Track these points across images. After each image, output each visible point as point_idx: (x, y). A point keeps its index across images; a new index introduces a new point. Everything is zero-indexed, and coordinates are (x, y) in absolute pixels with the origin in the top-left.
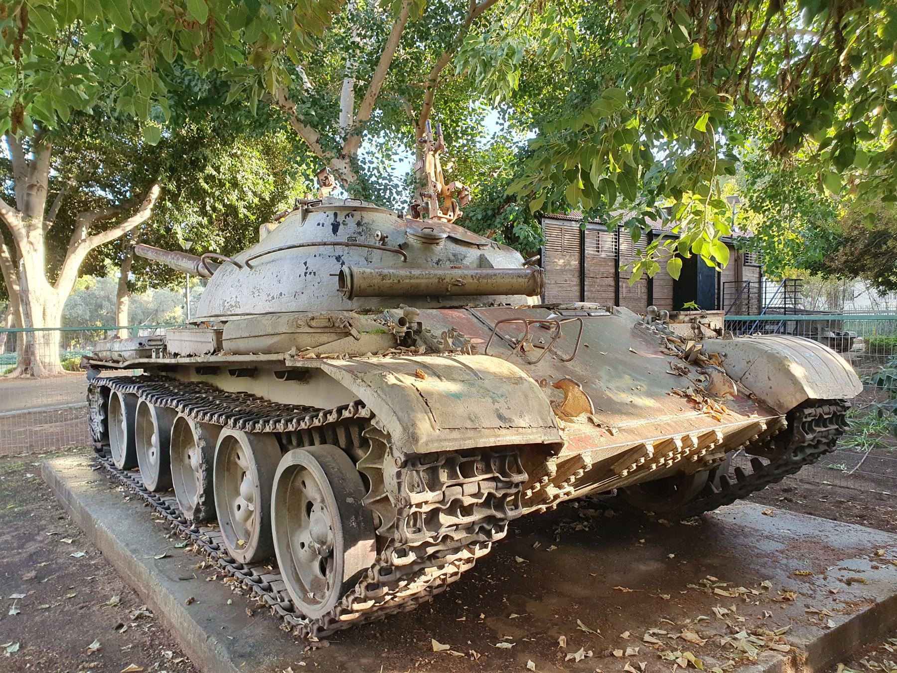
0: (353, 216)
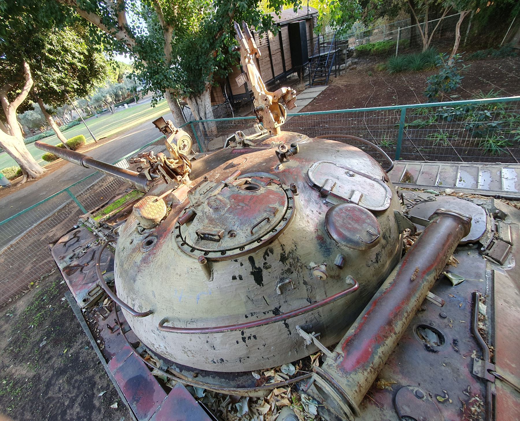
0: (272, 251)
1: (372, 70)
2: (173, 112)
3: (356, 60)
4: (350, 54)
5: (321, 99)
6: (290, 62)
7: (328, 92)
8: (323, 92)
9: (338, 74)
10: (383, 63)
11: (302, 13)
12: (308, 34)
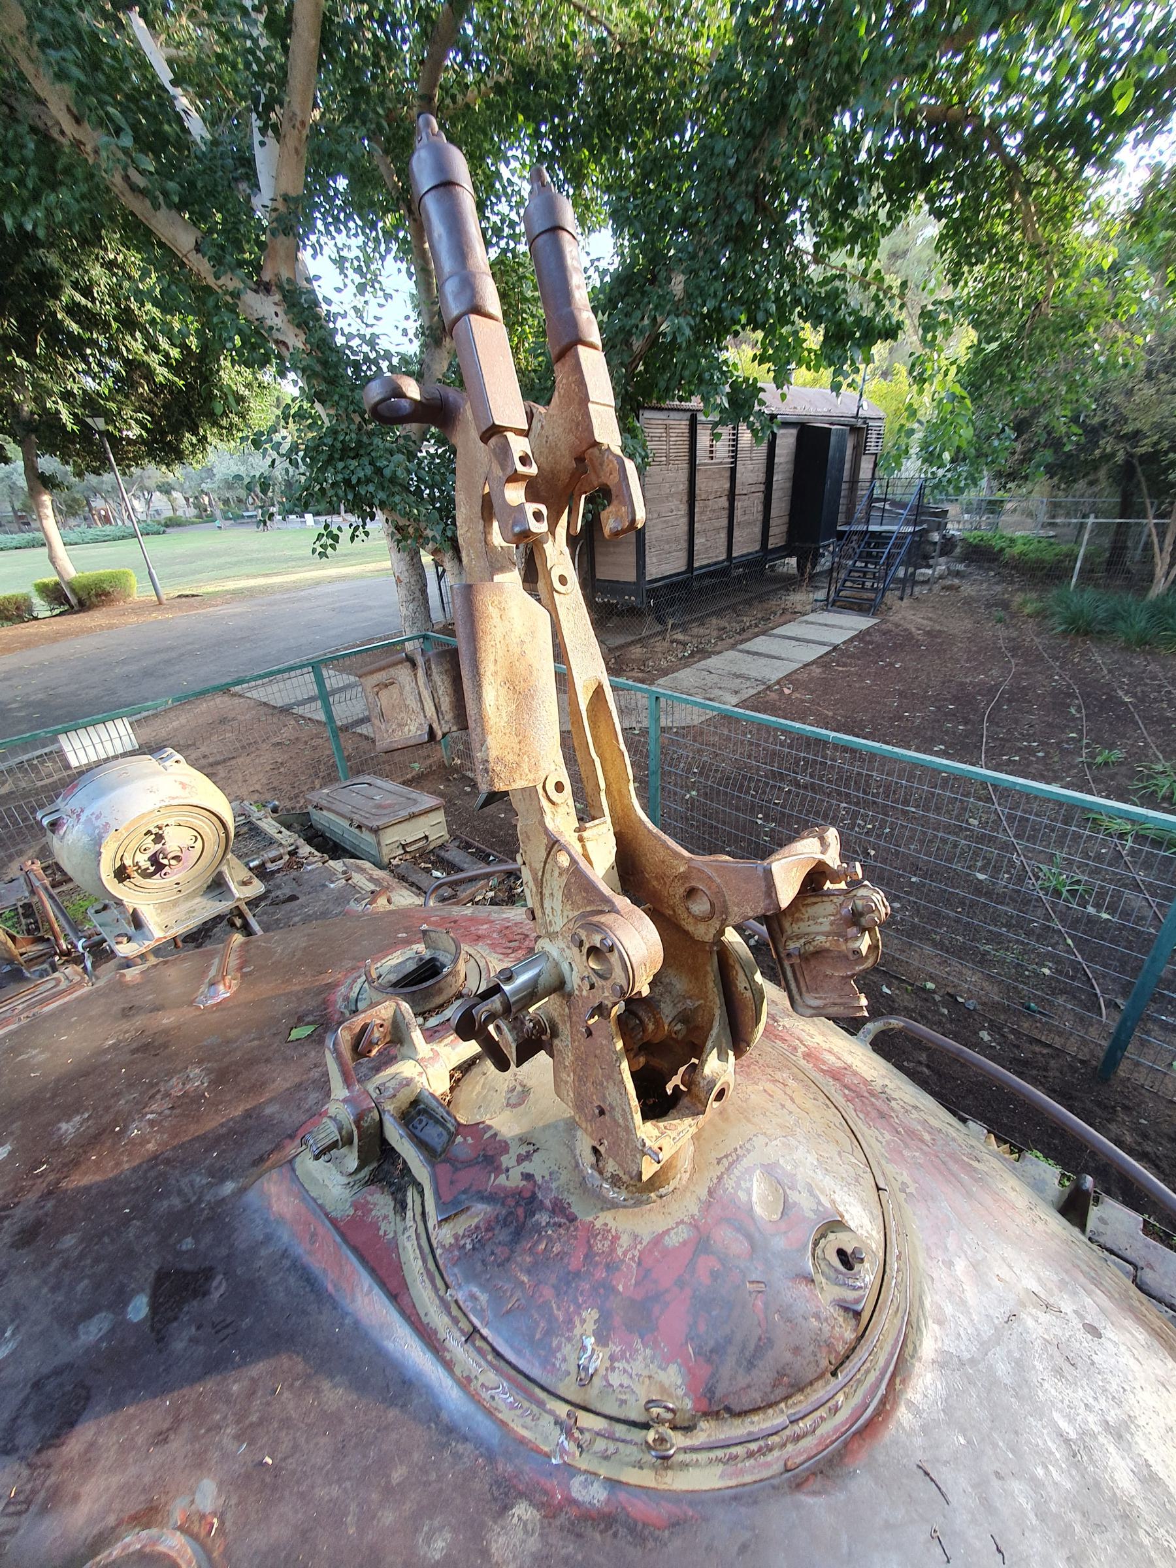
1: (1005, 605)
2: (399, 581)
3: (961, 567)
4: (948, 545)
5: (852, 656)
6: (784, 528)
7: (877, 638)
8: (861, 636)
9: (908, 591)
10: (1034, 595)
11: (844, 405)
12: (847, 466)
